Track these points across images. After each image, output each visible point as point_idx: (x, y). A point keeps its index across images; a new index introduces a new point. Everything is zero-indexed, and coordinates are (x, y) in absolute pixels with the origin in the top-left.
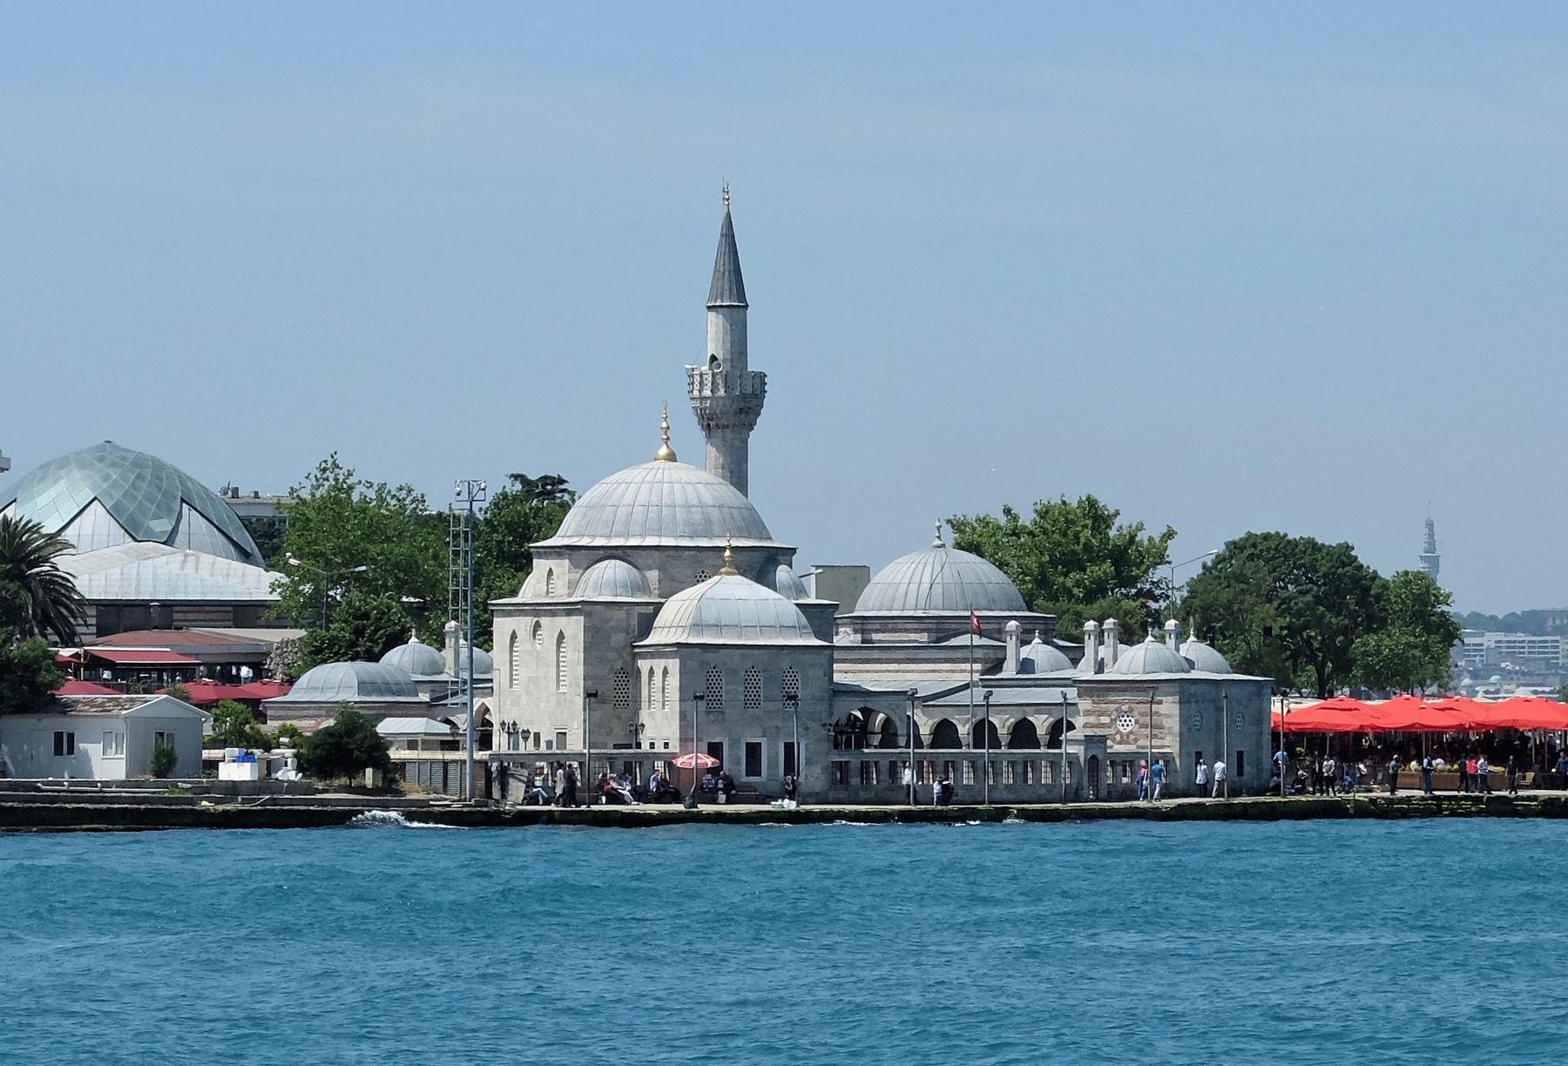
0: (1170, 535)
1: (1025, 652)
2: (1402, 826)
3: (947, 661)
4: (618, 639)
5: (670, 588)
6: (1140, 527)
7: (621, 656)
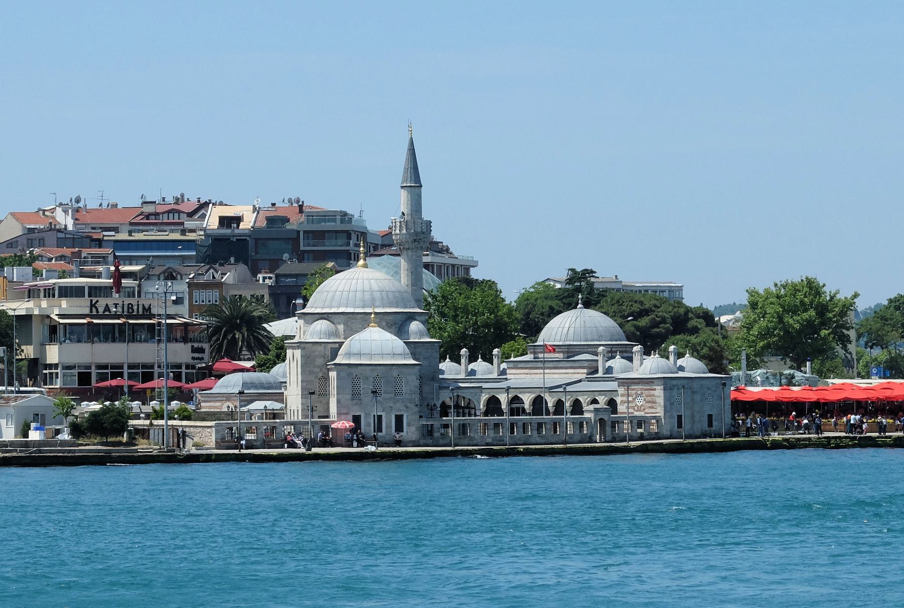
0: (856, 295)
3: (571, 368)
4: (320, 361)
5: (350, 331)
6: (837, 292)
7: (321, 370)
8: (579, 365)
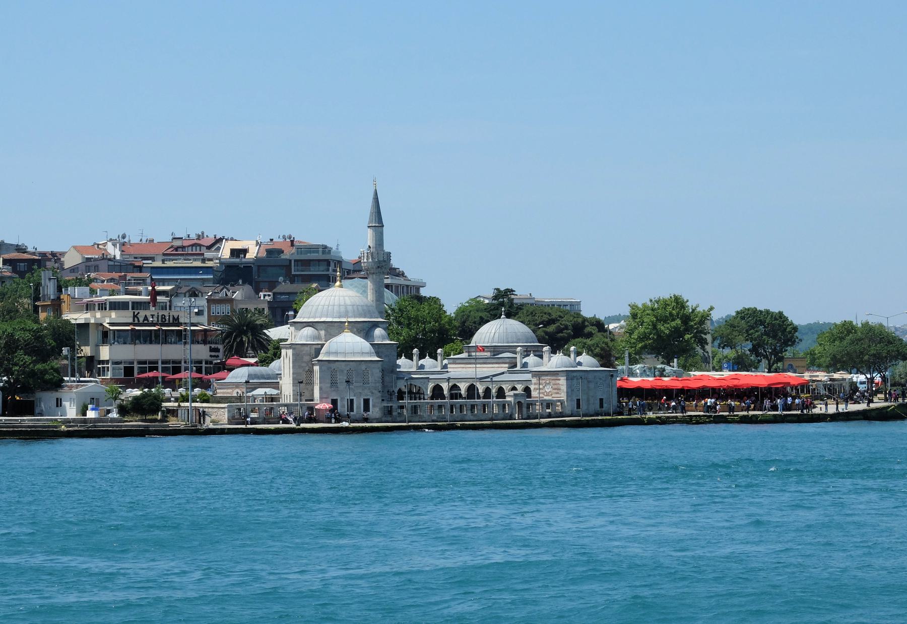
0: (711, 309)
1: (421, 362)
2: (696, 428)
4: (306, 358)
8: (502, 361)
